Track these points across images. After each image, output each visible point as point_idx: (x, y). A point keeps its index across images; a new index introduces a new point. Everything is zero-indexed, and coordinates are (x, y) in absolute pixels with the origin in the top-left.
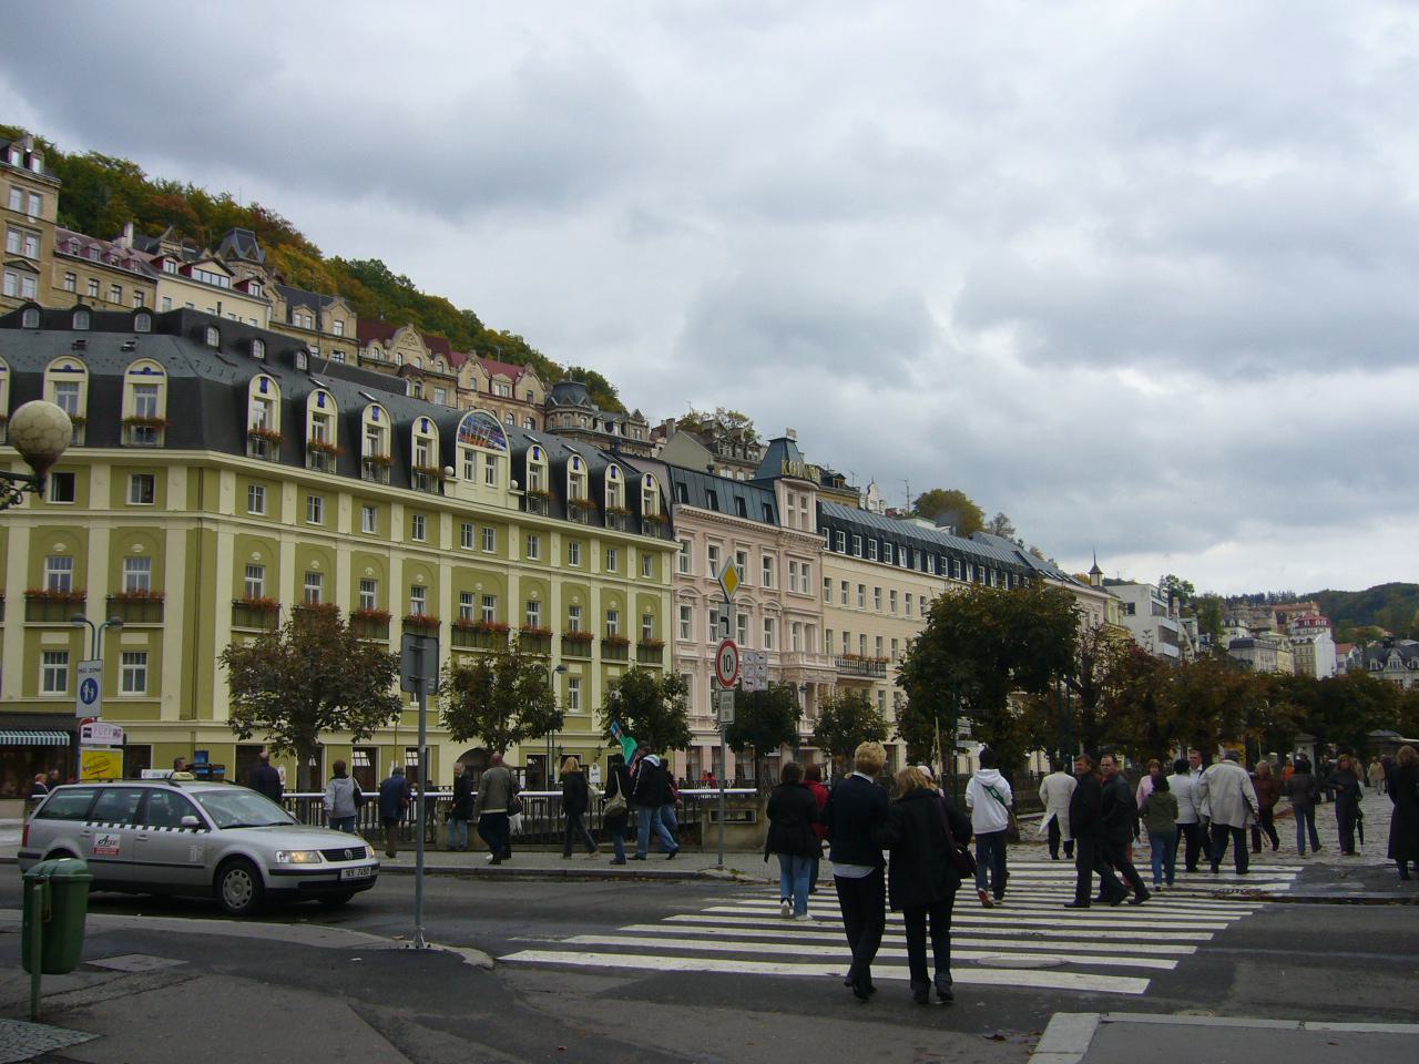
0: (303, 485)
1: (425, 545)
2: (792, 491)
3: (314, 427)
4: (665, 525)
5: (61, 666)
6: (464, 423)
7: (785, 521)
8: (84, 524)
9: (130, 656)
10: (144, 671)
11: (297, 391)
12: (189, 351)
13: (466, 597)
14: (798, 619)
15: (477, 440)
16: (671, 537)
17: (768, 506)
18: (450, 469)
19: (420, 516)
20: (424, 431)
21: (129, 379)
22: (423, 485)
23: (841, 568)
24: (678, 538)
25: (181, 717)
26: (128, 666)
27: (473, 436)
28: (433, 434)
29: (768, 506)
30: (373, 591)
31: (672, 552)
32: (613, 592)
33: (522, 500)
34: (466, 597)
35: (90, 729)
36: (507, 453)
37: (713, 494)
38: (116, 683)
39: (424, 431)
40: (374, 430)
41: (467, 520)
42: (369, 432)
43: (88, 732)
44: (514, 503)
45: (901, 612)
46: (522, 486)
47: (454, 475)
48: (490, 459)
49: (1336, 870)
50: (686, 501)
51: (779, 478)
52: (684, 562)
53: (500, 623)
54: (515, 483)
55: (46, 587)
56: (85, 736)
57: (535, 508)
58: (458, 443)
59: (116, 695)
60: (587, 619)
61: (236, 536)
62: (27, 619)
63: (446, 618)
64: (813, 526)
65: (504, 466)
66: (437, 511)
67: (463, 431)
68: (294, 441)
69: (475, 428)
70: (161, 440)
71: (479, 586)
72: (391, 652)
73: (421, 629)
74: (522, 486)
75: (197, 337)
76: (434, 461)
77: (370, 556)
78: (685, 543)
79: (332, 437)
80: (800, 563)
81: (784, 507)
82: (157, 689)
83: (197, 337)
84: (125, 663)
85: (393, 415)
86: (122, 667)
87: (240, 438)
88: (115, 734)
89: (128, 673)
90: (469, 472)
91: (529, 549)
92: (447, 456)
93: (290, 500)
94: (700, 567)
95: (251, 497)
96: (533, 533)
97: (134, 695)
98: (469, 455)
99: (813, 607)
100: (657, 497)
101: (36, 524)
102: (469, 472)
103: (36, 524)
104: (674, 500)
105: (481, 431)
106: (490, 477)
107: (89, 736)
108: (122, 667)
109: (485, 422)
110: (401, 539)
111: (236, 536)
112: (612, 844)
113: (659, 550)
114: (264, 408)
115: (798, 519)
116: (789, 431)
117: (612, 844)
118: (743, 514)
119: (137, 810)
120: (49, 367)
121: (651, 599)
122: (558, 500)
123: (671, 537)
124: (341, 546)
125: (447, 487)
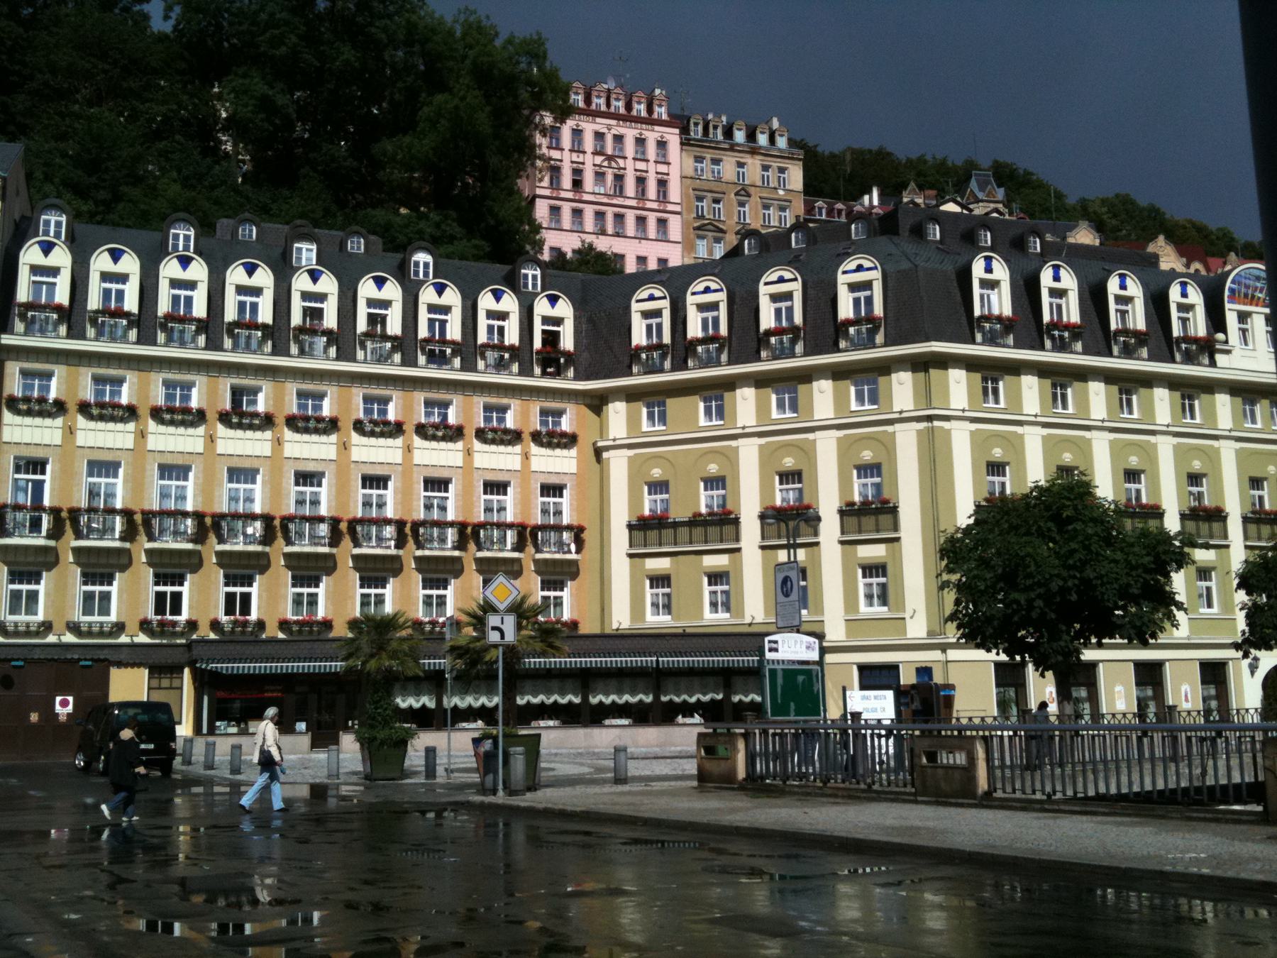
3: (1051, 305)
6: (1233, 282)
12: (909, 247)
18: (1220, 336)
22: (1189, 359)
27: (1246, 295)
28: (1195, 297)
30: (1004, 475)
35: (776, 642)
40: (1184, 308)
42: (1179, 311)
43: (774, 646)
47: (1226, 342)
53: (1213, 505)
55: (857, 498)
56: (770, 650)
58: (1228, 306)
59: (644, 620)
60: (1155, 487)
61: (1043, 437)
63: (1234, 510)
66: (1210, 387)
67: (1232, 291)
68: (1028, 322)
69: (1247, 287)
71: (1271, 469)
73: (1206, 517)
76: (1200, 327)
77: (997, 435)
80: (610, 212)
85: (1145, 286)
88: (808, 648)
91: (1245, 415)
98: (1243, 317)
105: (1256, 288)
107: (776, 650)
110: (1168, 420)
111: (1043, 437)
112: (1260, 808)
117: (1260, 808)
120: (763, 280)
121: (1004, 437)
124: (1159, 439)
125: (1218, 357)
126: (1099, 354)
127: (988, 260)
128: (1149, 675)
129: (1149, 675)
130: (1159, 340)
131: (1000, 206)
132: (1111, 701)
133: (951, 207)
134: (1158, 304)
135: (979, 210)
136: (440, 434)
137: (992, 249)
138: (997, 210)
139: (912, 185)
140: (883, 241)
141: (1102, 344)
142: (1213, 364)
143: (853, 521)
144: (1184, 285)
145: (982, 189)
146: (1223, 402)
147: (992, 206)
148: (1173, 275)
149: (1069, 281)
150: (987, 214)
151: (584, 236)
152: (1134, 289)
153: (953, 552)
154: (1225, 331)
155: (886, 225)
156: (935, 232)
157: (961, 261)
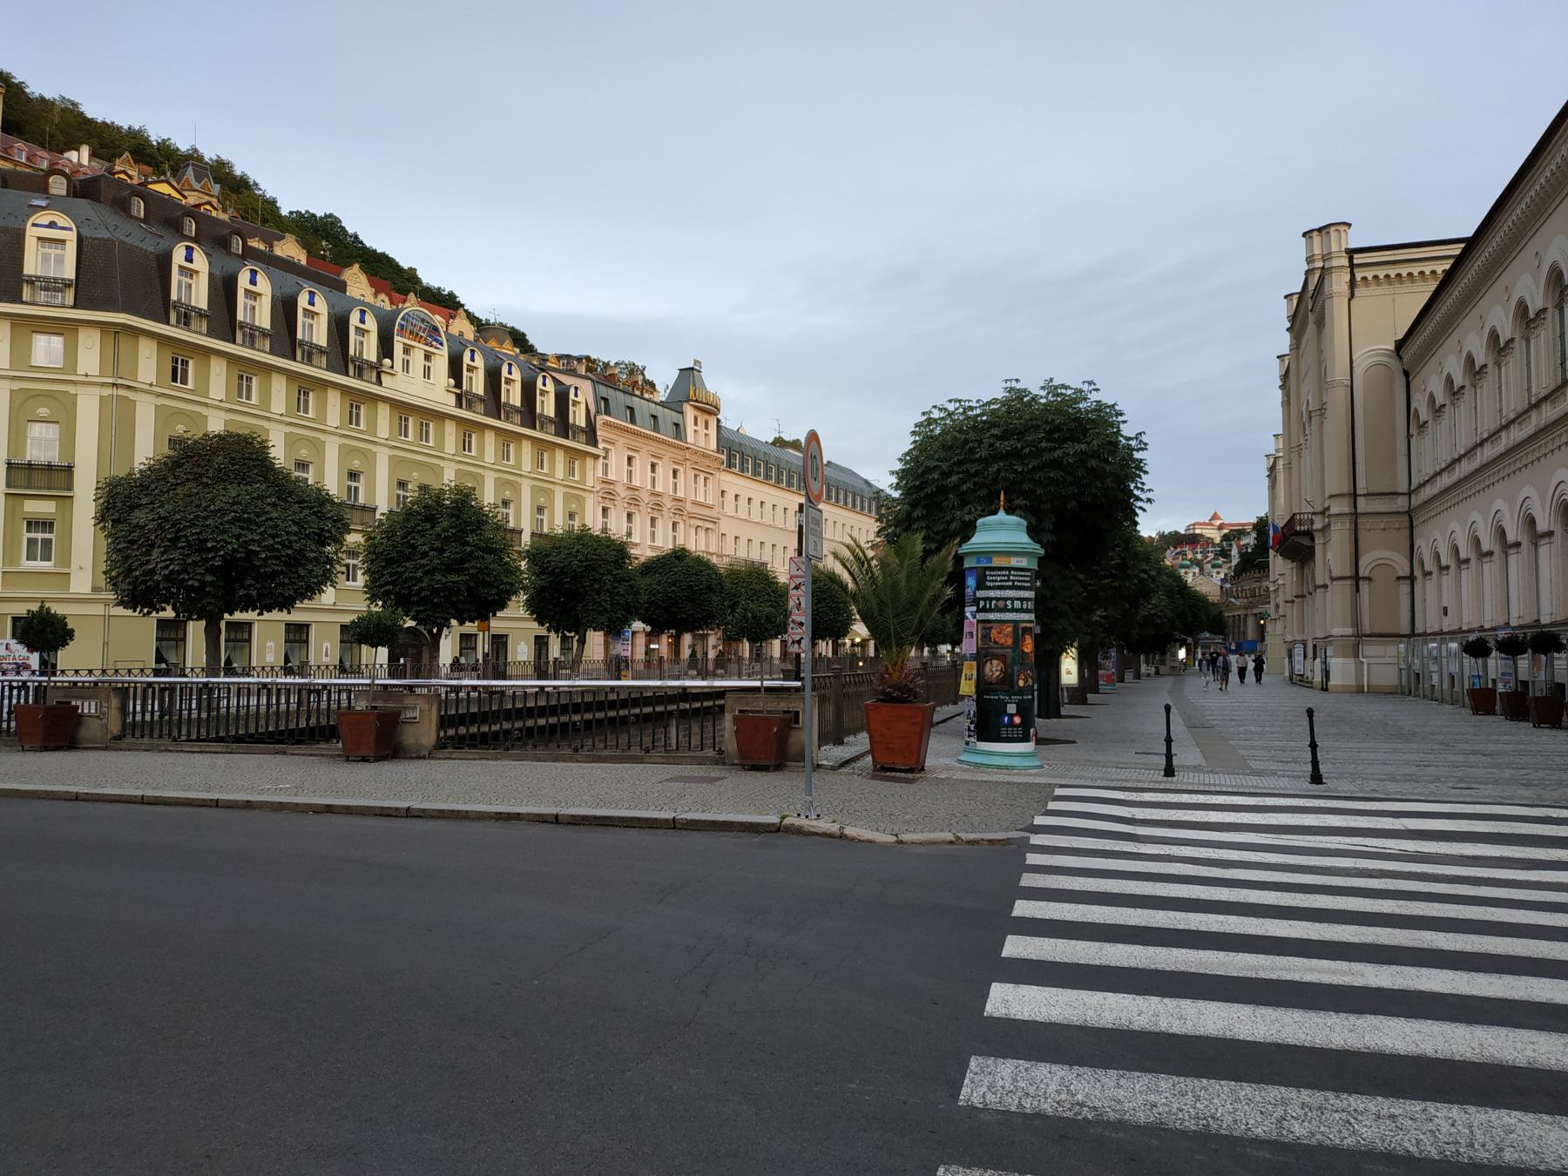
0: (345, 390)
1: (253, 406)
2: (698, 414)
3: (180, 282)
4: (591, 434)
5: (47, 536)
7: (690, 438)
8: (71, 389)
9: (32, 524)
10: (50, 541)
11: (287, 290)
12: (112, 218)
13: (402, 485)
14: (700, 523)
15: (417, 337)
16: (595, 444)
17: (677, 425)
18: (387, 361)
19: (356, 399)
20: (362, 321)
21: (31, 233)
22: (359, 374)
23: (734, 483)
24: (601, 445)
25: (94, 589)
26: (33, 535)
28: (371, 324)
29: (677, 425)
31: (596, 457)
32: (509, 482)
33: (459, 397)
34: (402, 485)
36: (445, 351)
37: (631, 409)
38: (20, 552)
39: (362, 321)
41: (403, 410)
44: (452, 399)
45: (742, 514)
46: (459, 385)
48: (428, 357)
49: (1014, 562)
50: (607, 412)
51: (688, 400)
52: (606, 471)
54: (452, 381)
57: (470, 407)
62: (8, 485)
64: (713, 446)
65: (441, 364)
67: (402, 326)
70: (70, 299)
72: (362, 541)
74: (459, 385)
75: (122, 206)
76: (371, 353)
78: (607, 451)
79: (264, 320)
81: (690, 427)
82: (66, 559)
83: (122, 206)
84: (29, 531)
85: (331, 305)
86: (26, 536)
87: (161, 306)
89: (31, 542)
90: (406, 364)
92: (386, 348)
93: (334, 406)
94: (617, 471)
95: (240, 386)
96: (468, 429)
97: (39, 565)
98: (407, 350)
99: (713, 514)
100: (583, 407)
101: (16, 386)
102: (406, 364)
103: (16, 386)
104: (598, 412)
106: (427, 373)
108: (26, 536)
109: (423, 321)
110: (337, 424)
113: (586, 454)
114: (192, 277)
115: (702, 437)
116: (696, 362)
118: (633, 421)
119: (626, 622)
122: (493, 401)
123: (595, 444)
125: (384, 378)
126: (284, 356)
127: (189, 250)
128: (298, 634)
129: (298, 634)
130: (339, 352)
131: (214, 201)
132: (262, 655)
133: (164, 188)
134: (339, 326)
135: (192, 199)
136: (80, 157)
137: (195, 240)
138: (209, 203)
139: (127, 155)
140: (82, 203)
141: (288, 351)
142: (379, 382)
143: (22, 476)
144: (363, 312)
145: (198, 180)
146: (384, 412)
147: (207, 198)
148: (355, 302)
149: (264, 286)
150: (198, 206)
151: (1339, 535)
152: (321, 306)
153: (119, 502)
154: (392, 359)
155: (83, 189)
156: (139, 208)
157: (164, 244)
